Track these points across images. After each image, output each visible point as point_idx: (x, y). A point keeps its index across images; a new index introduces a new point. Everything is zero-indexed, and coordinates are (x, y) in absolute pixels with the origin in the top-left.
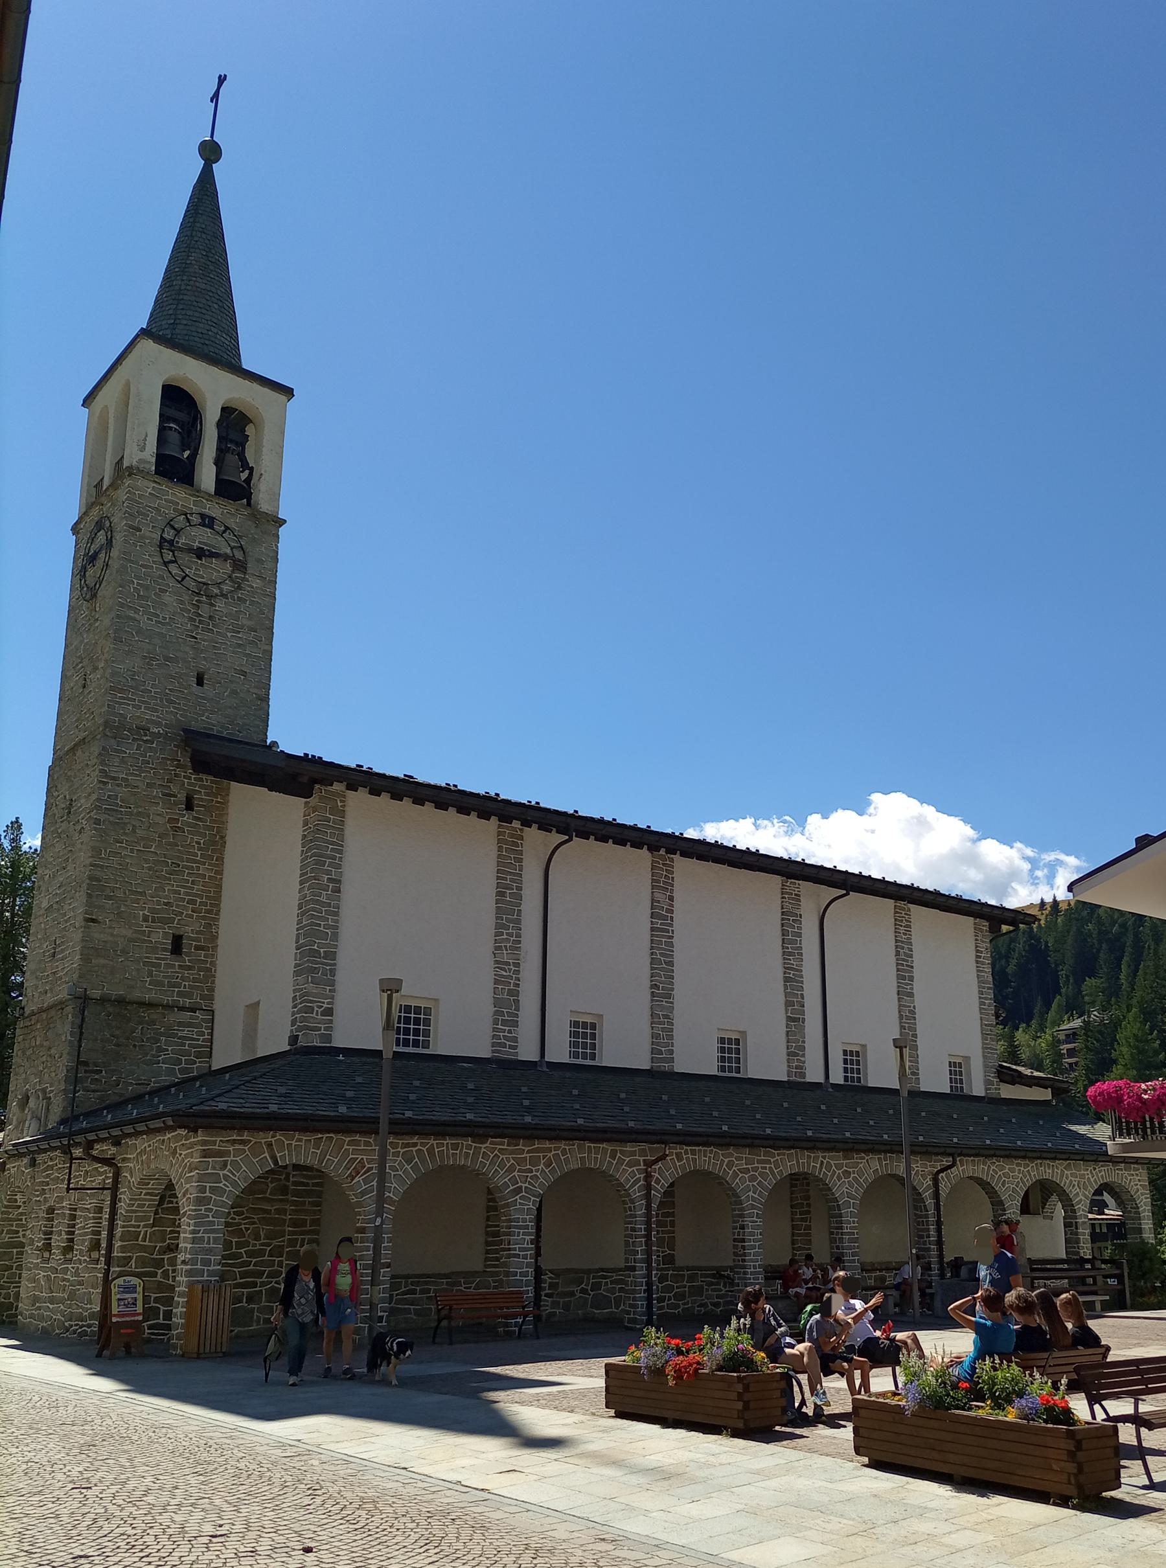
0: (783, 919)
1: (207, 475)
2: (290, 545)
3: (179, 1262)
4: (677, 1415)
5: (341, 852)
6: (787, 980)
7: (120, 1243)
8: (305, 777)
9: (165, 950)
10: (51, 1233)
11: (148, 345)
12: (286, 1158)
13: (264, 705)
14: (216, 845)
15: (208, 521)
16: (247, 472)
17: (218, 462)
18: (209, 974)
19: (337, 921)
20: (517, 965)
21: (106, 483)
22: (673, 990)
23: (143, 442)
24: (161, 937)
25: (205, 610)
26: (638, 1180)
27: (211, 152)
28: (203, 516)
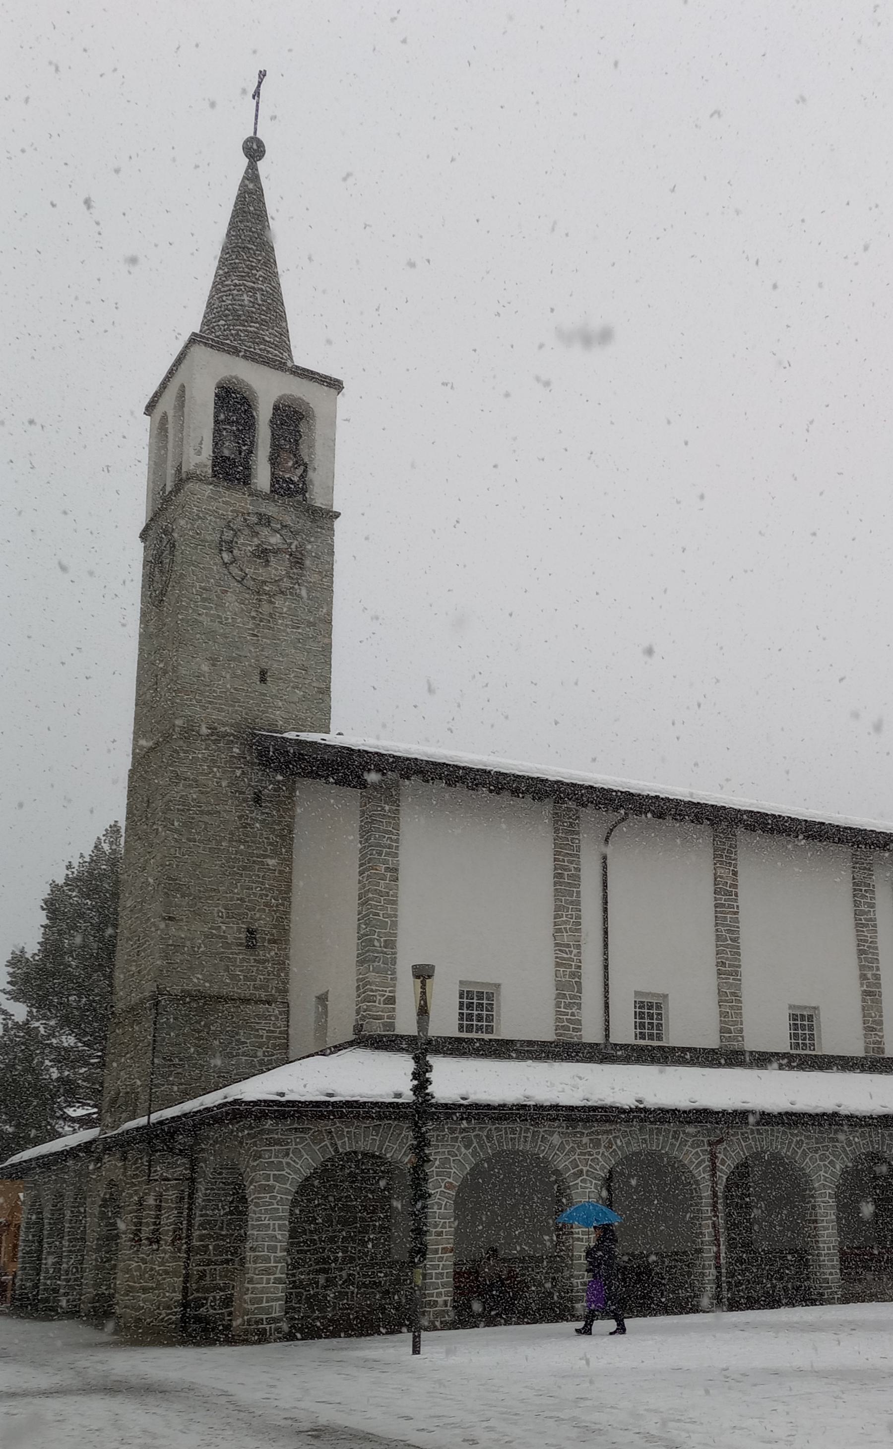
0: (855, 890)
1: (262, 477)
2: (345, 537)
3: (248, 1249)
4: (368, 1446)
5: (397, 841)
6: (861, 952)
7: (198, 1233)
8: (348, 768)
9: (241, 944)
10: (141, 1224)
11: (199, 352)
12: (345, 1145)
13: (326, 697)
14: (285, 838)
15: (265, 520)
16: (302, 467)
17: (274, 461)
18: (282, 965)
19: (396, 910)
20: (578, 947)
21: (168, 489)
22: (739, 966)
23: (199, 448)
24: (234, 932)
25: (266, 608)
26: (703, 1161)
27: (254, 150)
28: (260, 515)
